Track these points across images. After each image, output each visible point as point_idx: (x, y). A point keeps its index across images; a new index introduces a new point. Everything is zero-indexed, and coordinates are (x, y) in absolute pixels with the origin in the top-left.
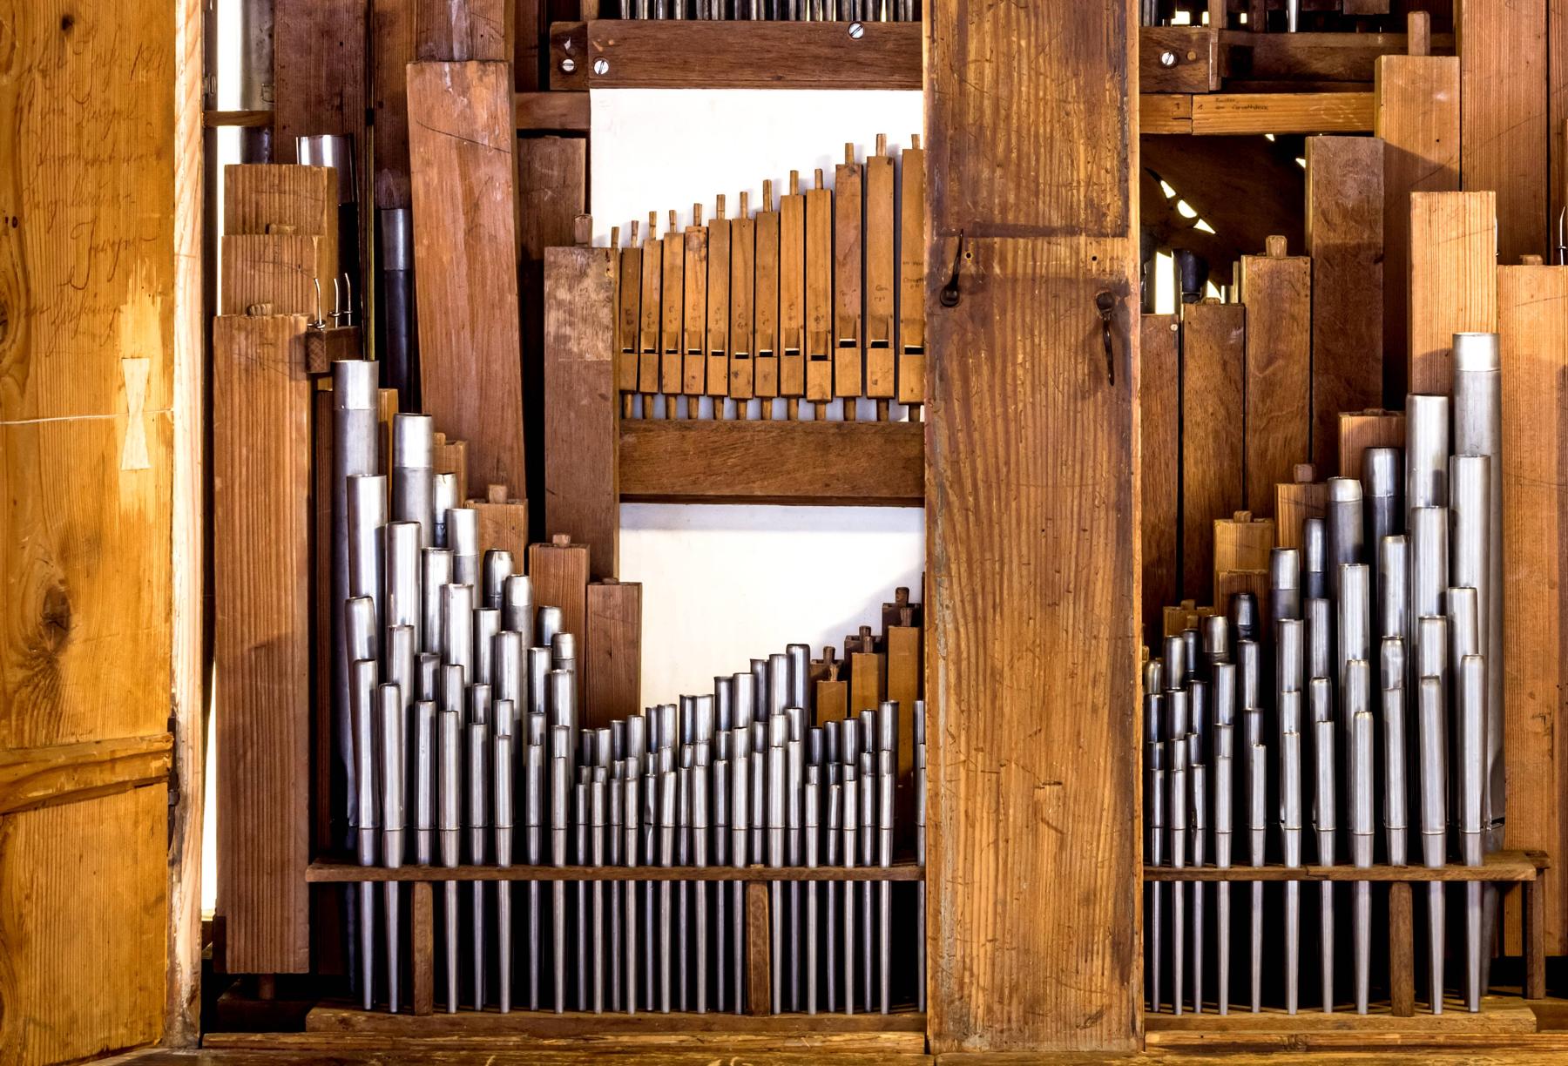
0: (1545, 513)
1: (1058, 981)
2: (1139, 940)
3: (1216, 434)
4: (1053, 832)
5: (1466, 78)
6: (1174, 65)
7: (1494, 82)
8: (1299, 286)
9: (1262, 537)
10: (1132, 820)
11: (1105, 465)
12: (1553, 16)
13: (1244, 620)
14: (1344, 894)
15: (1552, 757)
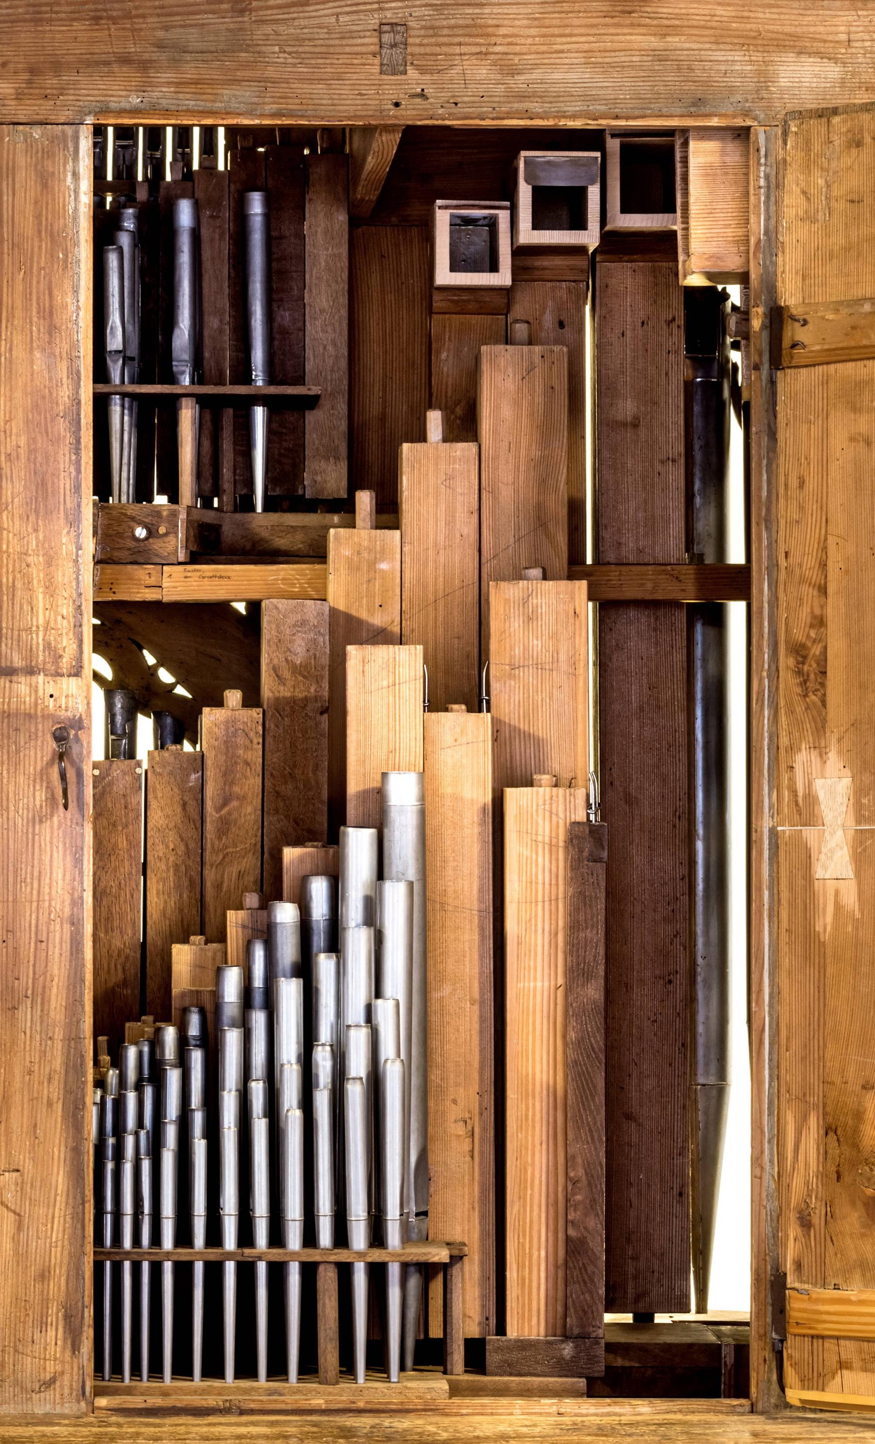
0: (467, 937)
1: (16, 1351)
2: (89, 1313)
3: (176, 867)
4: (11, 1214)
5: (406, 549)
6: (146, 539)
7: (431, 552)
8: (252, 734)
9: (214, 959)
10: (83, 1204)
11: (60, 882)
12: (484, 492)
13: (194, 1030)
14: (278, 1272)
15: (472, 1157)
